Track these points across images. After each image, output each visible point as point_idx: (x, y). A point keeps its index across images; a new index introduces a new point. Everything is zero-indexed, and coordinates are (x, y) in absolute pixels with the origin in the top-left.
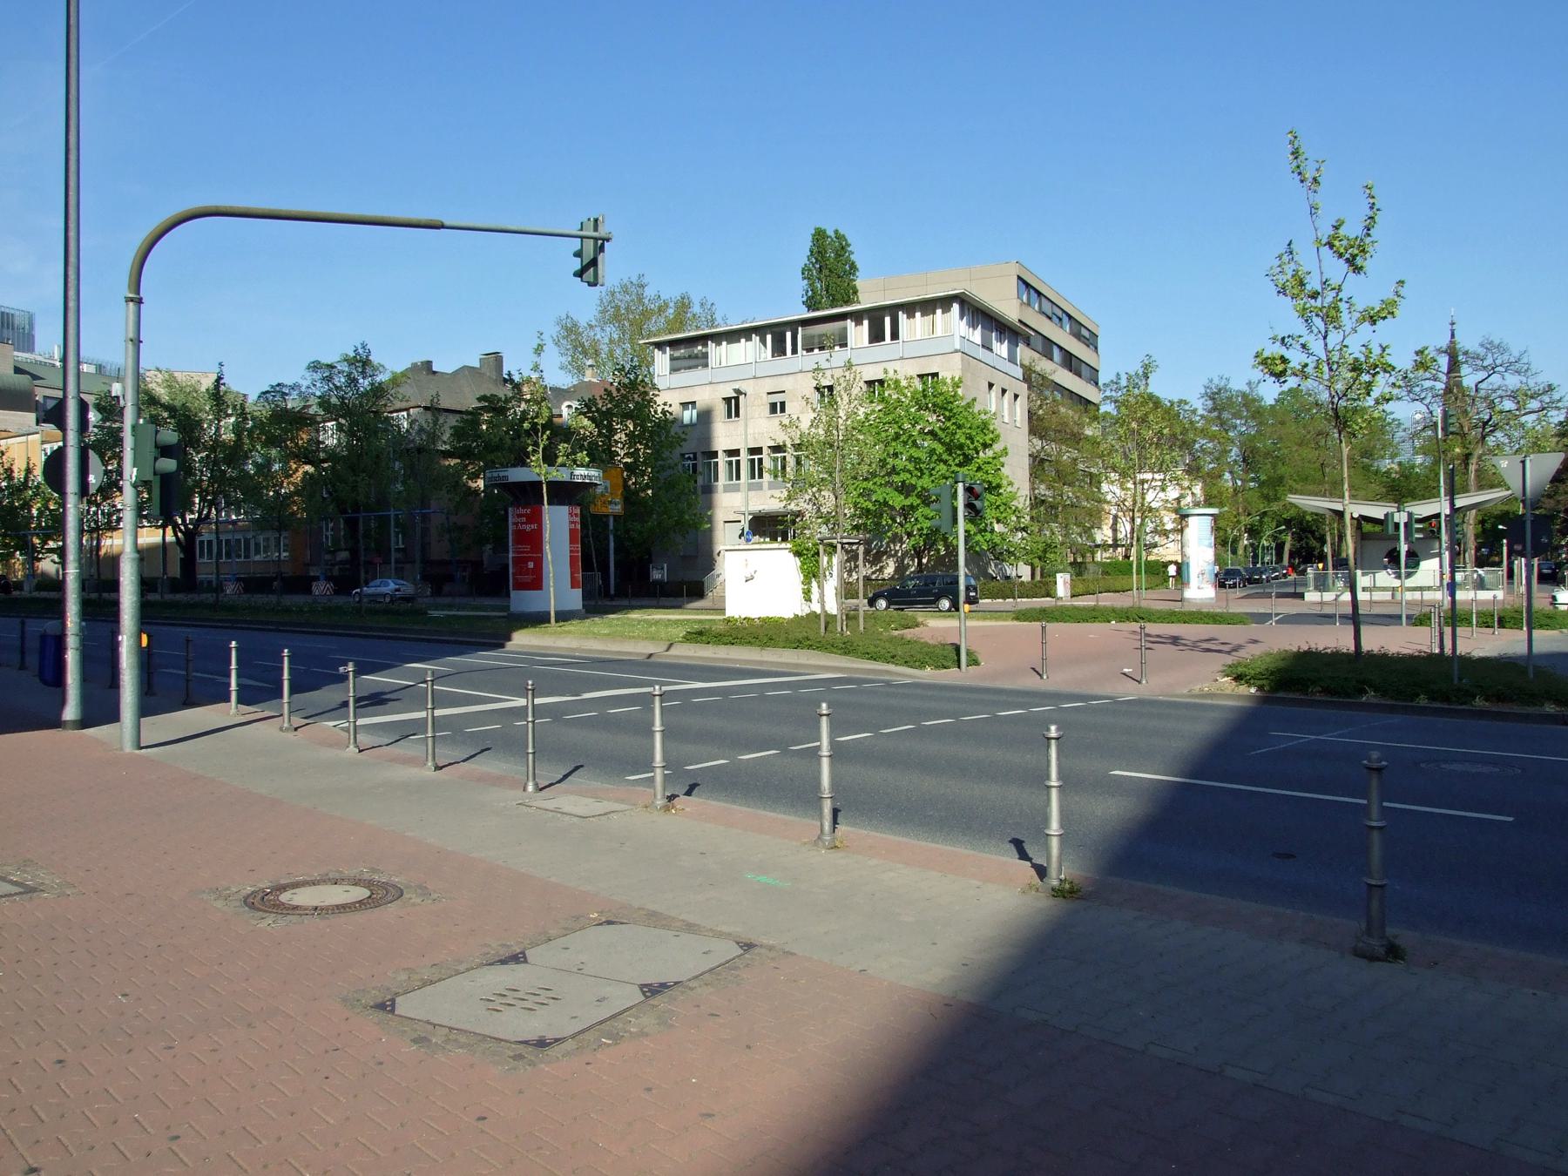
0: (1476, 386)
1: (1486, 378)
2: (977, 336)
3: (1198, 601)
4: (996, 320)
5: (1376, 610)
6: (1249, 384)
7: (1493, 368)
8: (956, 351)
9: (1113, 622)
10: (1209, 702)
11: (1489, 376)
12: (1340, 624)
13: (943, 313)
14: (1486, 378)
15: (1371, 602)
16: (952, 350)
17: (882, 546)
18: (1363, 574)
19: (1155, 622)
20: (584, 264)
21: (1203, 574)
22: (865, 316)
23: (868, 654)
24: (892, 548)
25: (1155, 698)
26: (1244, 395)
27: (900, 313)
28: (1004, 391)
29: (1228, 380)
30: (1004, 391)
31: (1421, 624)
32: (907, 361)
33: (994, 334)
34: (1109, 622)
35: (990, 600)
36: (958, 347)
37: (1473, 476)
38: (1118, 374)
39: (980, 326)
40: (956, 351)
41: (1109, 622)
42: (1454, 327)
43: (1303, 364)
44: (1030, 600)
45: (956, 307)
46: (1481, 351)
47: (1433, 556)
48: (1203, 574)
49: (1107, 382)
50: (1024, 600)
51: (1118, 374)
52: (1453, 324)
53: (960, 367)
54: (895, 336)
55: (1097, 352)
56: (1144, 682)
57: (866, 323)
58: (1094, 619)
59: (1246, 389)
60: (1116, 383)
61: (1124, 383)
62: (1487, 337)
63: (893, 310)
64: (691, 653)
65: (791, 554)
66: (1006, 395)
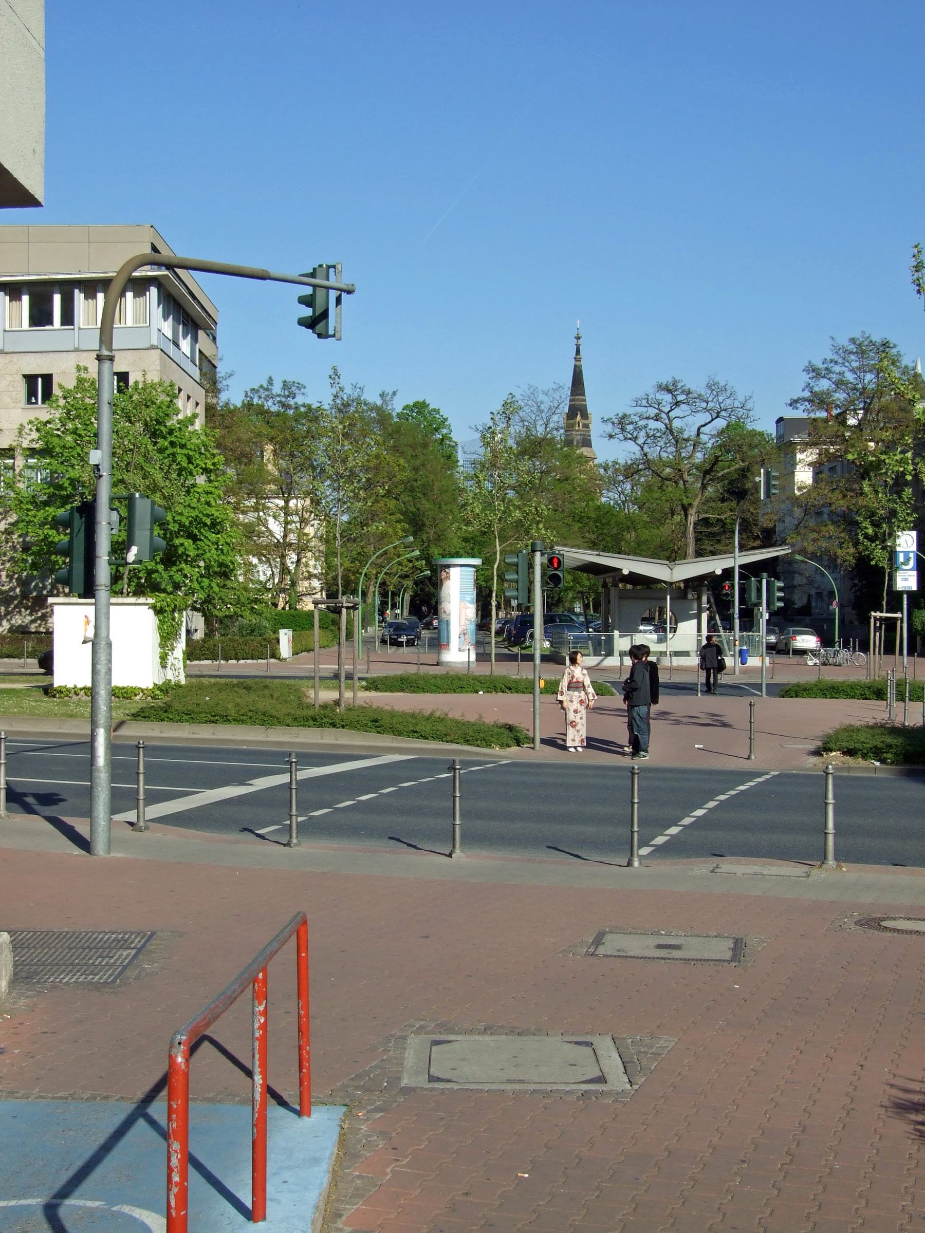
0: (699, 429)
1: (710, 422)
2: (167, 327)
3: (459, 666)
4: (185, 311)
5: (677, 679)
6: (382, 395)
7: (718, 413)
8: (153, 348)
9: (481, 693)
10: (846, 774)
11: (713, 420)
12: (702, 695)
13: (134, 297)
14: (710, 422)
15: (671, 669)
16: (147, 345)
17: (44, 587)
18: (621, 636)
19: (523, 692)
20: (324, 322)
21: (465, 634)
22: (24, 289)
23: (416, 732)
24: (61, 590)
25: (790, 772)
26: (378, 409)
27: (77, 291)
28: (189, 397)
29: (362, 389)
30: (189, 397)
31: (797, 696)
32: (84, 354)
33: (181, 327)
34: (477, 692)
35: (209, 662)
36: (155, 342)
37: (691, 529)
38: (270, 378)
39: (171, 316)
40: (153, 348)
41: (477, 692)
42: (580, 341)
43: (620, 415)
44: (255, 661)
45: (154, 291)
46: (704, 391)
47: (689, 618)
48: (465, 634)
49: (256, 388)
50: (249, 661)
51: (270, 378)
52: (578, 338)
53: (158, 368)
54: (68, 318)
55: (215, 343)
56: (753, 757)
57: (26, 299)
58: (461, 689)
59: (379, 402)
60: (267, 390)
61: (277, 389)
62: (713, 377)
63: (67, 287)
64: (156, 733)
65: (151, 612)
66: (191, 400)
